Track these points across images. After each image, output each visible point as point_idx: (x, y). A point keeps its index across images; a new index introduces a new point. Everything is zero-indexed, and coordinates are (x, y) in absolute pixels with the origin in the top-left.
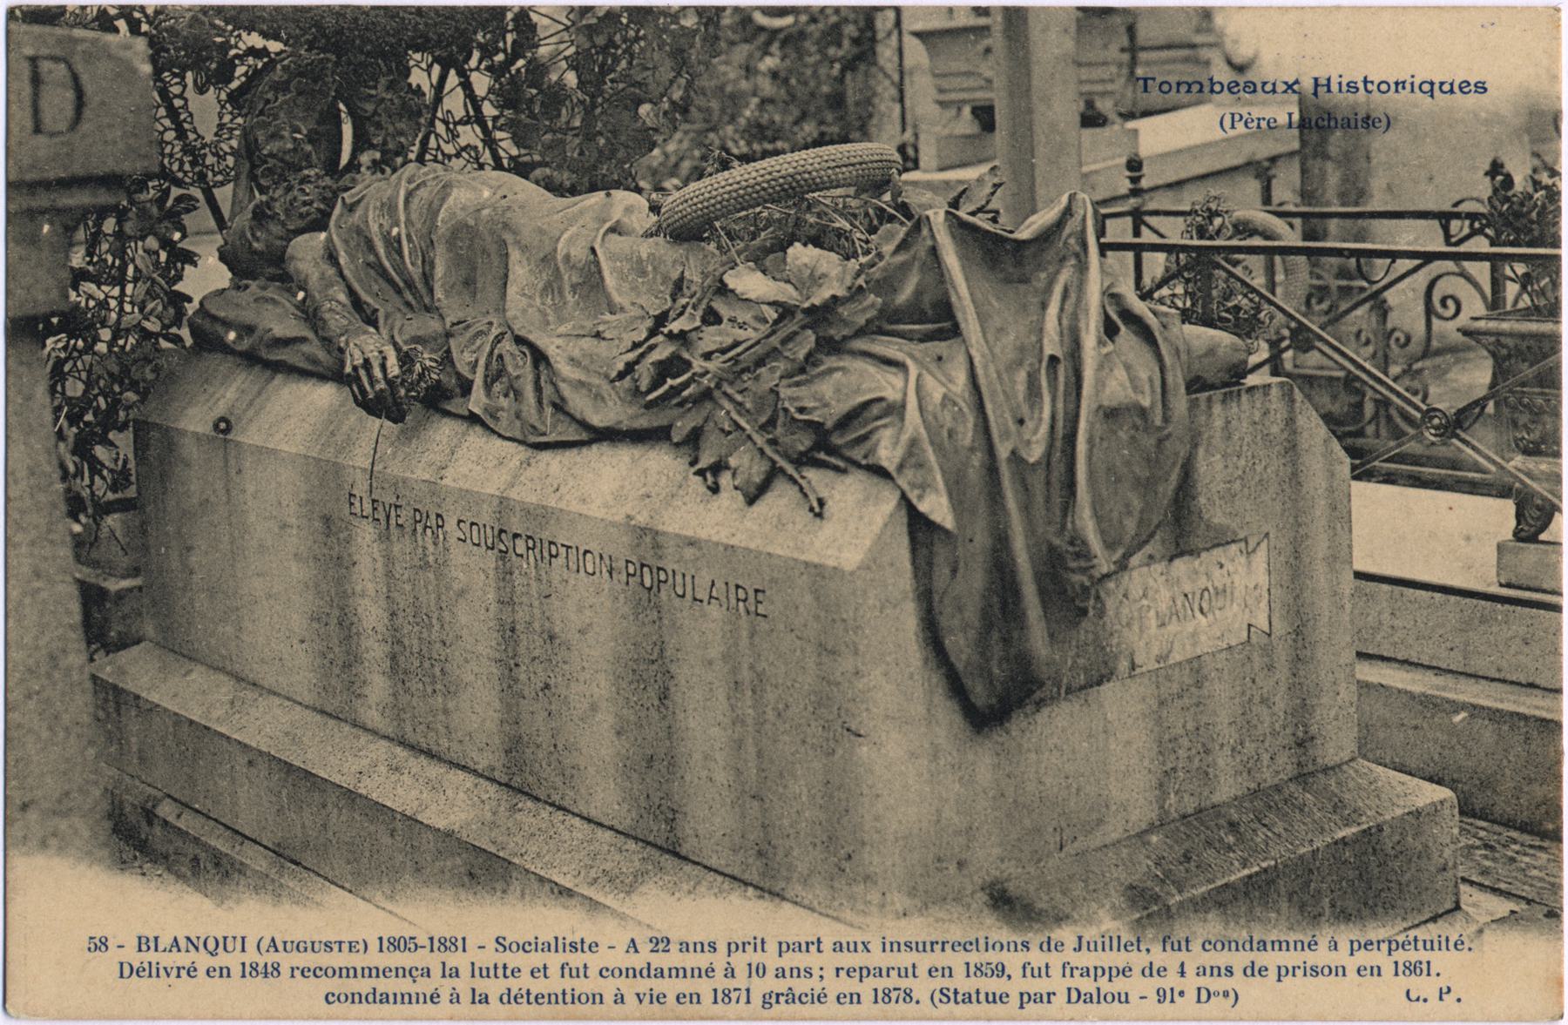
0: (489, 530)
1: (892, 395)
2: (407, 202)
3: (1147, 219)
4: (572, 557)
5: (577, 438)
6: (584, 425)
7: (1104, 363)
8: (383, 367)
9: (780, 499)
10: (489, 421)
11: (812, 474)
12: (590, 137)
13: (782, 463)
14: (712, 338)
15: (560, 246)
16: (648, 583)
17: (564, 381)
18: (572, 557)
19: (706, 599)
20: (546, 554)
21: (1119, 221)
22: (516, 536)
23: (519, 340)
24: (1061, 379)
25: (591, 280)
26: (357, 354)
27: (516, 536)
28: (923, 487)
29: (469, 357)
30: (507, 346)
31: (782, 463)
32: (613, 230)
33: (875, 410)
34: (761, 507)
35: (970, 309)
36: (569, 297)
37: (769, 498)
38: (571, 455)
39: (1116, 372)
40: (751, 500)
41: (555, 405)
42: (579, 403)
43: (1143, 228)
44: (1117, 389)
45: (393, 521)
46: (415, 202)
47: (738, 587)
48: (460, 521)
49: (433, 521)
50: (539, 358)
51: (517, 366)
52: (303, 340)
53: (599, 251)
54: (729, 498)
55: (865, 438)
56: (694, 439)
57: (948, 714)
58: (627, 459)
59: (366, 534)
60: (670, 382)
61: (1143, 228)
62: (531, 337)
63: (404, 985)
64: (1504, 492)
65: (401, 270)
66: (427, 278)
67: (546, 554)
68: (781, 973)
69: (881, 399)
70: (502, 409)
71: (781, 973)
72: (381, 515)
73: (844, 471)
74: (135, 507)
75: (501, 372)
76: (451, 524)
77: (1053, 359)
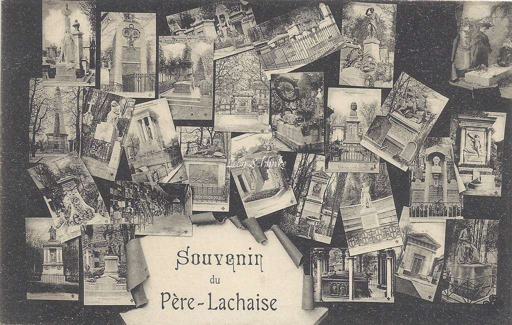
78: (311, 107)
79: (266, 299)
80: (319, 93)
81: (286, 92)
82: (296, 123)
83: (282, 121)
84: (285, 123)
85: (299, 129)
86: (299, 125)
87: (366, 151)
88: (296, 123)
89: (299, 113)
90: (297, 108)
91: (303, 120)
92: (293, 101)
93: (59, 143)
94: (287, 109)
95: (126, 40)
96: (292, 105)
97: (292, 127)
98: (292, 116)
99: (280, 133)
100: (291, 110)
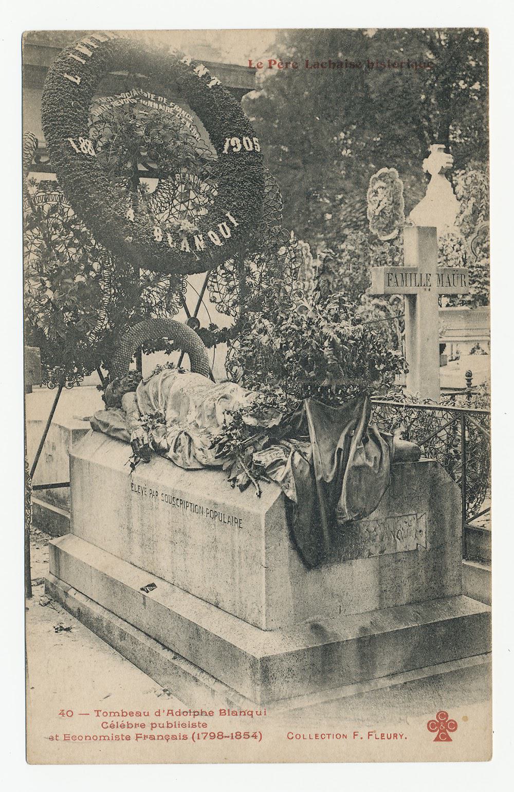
4: (192, 507)
5: (198, 467)
7: (358, 451)
8: (143, 440)
9: (251, 492)
10: (174, 461)
12: (364, 348)
13: (252, 479)
18: (192, 507)
22: (177, 499)
23: (186, 434)
24: (342, 456)
27: (177, 499)
28: (287, 488)
31: (252, 479)
32: (222, 397)
33: (278, 463)
34: (245, 492)
35: (313, 427)
36: (206, 419)
37: (248, 490)
38: (196, 473)
39: (362, 455)
40: (242, 490)
44: (361, 460)
46: (165, 383)
49: (155, 494)
50: (191, 440)
52: (123, 429)
54: (237, 489)
55: (275, 472)
56: (229, 470)
57: (297, 563)
62: (189, 434)
64: (126, 442)
72: (140, 491)
73: (269, 483)
74: (69, 486)
76: (160, 495)
77: (340, 450)
78: (367, 309)
79: (260, 492)
80: (438, 187)
81: (151, 184)
82: (233, 454)
83: (112, 435)
84: (146, 453)
85: (262, 503)
86: (262, 473)
87: (453, 396)
88: (233, 454)
89: (253, 368)
90: (242, 326)
91: (292, 430)
92: (205, 262)
93: (342, 260)
94: (164, 338)
95: (38, 181)
96: (204, 301)
97: (209, 488)
98: (200, 396)
99: (94, 550)
100: (190, 344)
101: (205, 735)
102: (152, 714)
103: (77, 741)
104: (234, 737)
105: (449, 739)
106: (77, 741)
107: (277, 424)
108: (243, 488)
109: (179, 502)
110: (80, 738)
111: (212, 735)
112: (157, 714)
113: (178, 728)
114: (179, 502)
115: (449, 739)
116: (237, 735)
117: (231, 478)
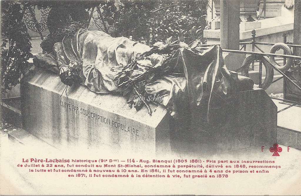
0: (87, 111)
1: (168, 89)
2: (79, 36)
3: (258, 45)
6: (107, 90)
9: (143, 111)
11: (150, 105)
14: (135, 73)
15: (108, 49)
16: (116, 126)
17: (104, 80)
19: (127, 131)
20: (97, 118)
21: (249, 45)
22: (92, 113)
25: (113, 59)
26: (62, 70)
29: (86, 73)
30: (94, 71)
34: (139, 112)
41: (102, 85)
42: (107, 85)
43: (255, 48)
45: (69, 107)
47: (133, 129)
48: (81, 109)
51: (95, 76)
53: (115, 51)
54: (134, 109)
58: (115, 98)
59: (63, 110)
60: (124, 82)
61: (255, 48)
63: (108, 173)
65: (76, 51)
66: (81, 55)
67: (97, 118)
68: (178, 171)
69: (166, 90)
70: (92, 85)
71: (178, 171)
75: (92, 77)
101: (223, 176)
102: (255, 172)
103: (147, 167)
104: (236, 167)
105: (278, 155)
106: (147, 167)
107: (160, 65)
108: (138, 109)
109: (92, 115)
110: (106, 176)
111: (156, 171)
112: (18, 166)
113: (129, 167)
114: (92, 115)
115: (278, 155)
116: (78, 175)
117: (129, 101)
